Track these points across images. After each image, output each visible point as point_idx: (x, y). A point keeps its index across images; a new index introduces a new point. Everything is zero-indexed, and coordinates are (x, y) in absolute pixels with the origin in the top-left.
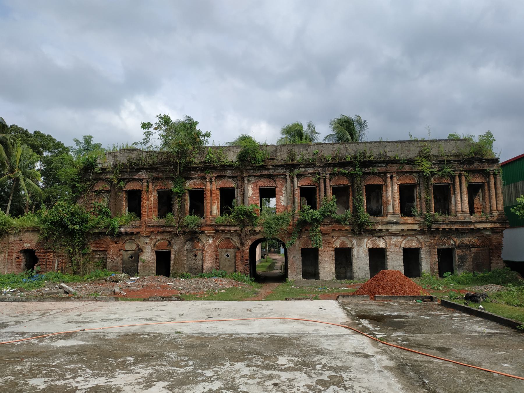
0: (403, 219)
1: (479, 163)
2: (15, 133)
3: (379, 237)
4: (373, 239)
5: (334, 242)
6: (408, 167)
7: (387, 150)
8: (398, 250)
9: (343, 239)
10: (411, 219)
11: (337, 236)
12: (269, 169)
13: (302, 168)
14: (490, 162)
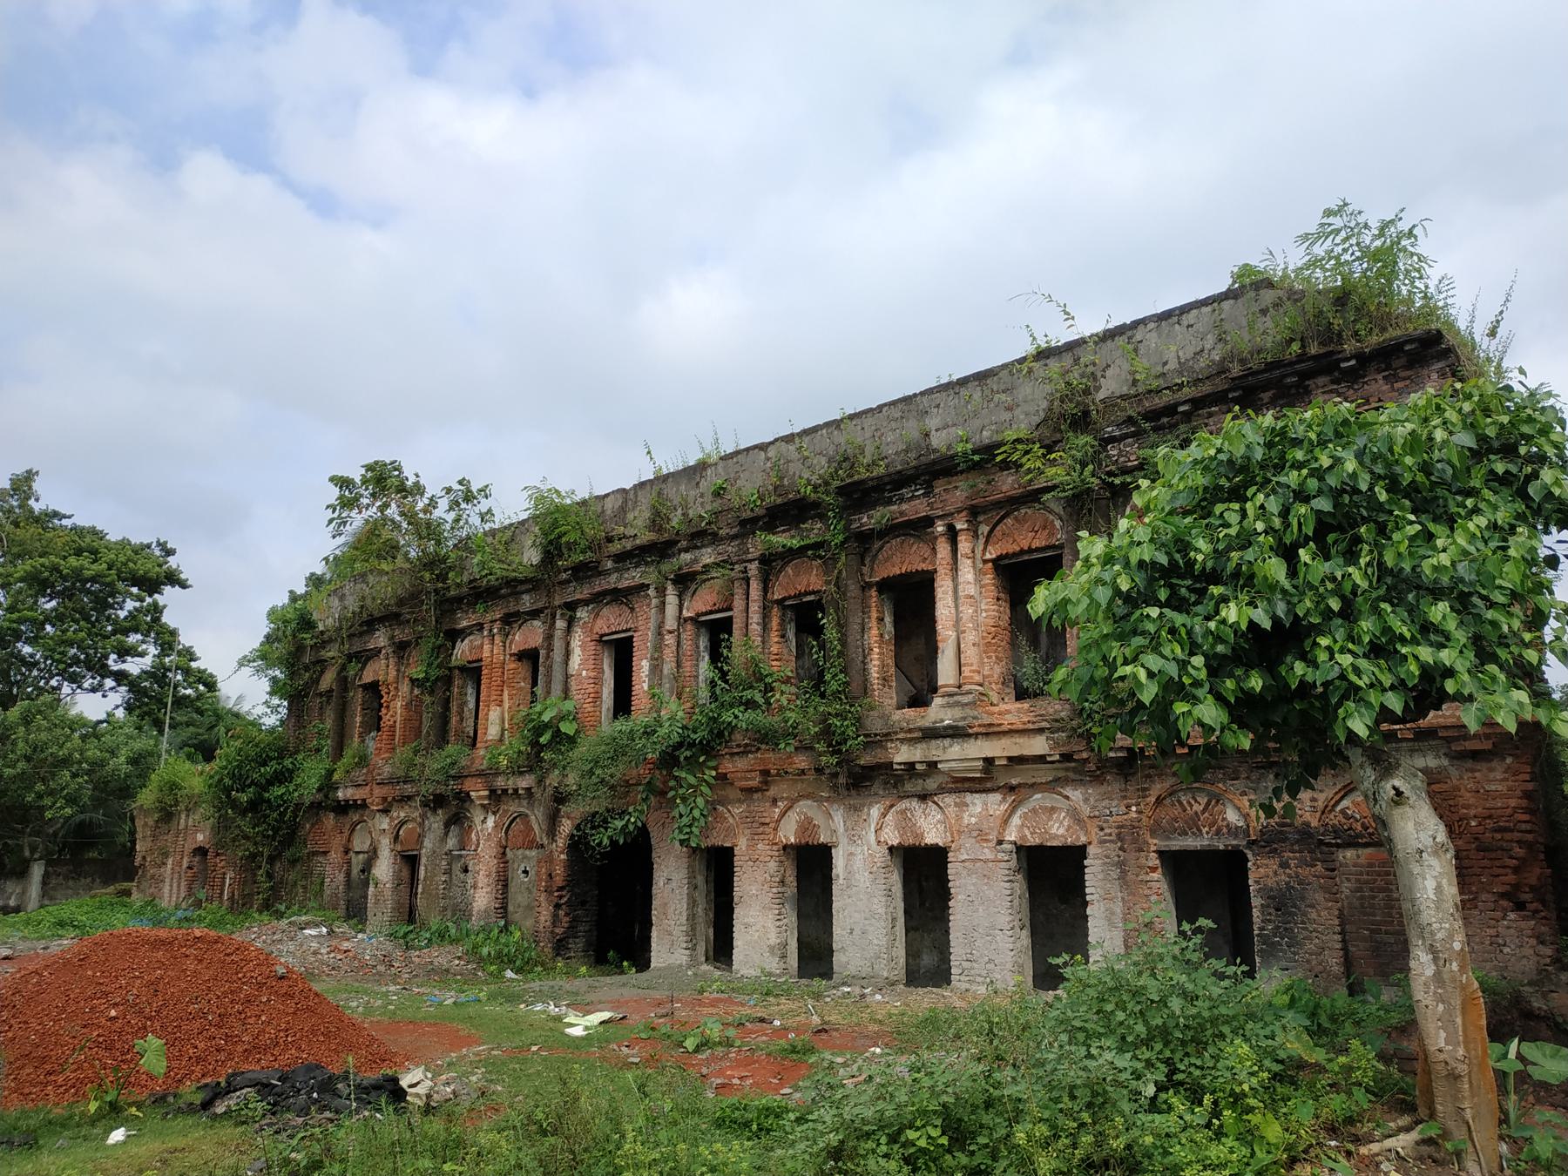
0: (986, 712)
1: (1333, 382)
2: (117, 616)
3: (923, 797)
4: (904, 804)
5: (778, 821)
6: (1010, 480)
7: (932, 423)
8: (988, 854)
9: (806, 807)
10: (1019, 711)
11: (787, 799)
12: (607, 573)
13: (686, 550)
14: (1396, 363)
